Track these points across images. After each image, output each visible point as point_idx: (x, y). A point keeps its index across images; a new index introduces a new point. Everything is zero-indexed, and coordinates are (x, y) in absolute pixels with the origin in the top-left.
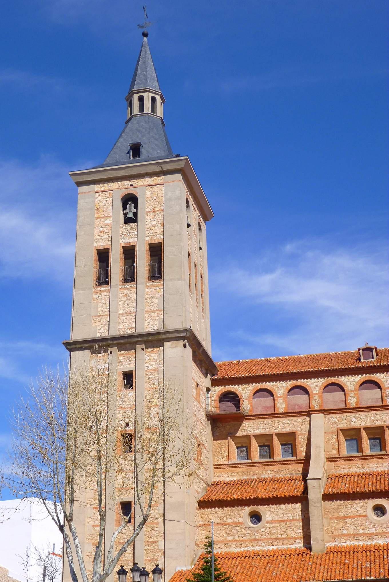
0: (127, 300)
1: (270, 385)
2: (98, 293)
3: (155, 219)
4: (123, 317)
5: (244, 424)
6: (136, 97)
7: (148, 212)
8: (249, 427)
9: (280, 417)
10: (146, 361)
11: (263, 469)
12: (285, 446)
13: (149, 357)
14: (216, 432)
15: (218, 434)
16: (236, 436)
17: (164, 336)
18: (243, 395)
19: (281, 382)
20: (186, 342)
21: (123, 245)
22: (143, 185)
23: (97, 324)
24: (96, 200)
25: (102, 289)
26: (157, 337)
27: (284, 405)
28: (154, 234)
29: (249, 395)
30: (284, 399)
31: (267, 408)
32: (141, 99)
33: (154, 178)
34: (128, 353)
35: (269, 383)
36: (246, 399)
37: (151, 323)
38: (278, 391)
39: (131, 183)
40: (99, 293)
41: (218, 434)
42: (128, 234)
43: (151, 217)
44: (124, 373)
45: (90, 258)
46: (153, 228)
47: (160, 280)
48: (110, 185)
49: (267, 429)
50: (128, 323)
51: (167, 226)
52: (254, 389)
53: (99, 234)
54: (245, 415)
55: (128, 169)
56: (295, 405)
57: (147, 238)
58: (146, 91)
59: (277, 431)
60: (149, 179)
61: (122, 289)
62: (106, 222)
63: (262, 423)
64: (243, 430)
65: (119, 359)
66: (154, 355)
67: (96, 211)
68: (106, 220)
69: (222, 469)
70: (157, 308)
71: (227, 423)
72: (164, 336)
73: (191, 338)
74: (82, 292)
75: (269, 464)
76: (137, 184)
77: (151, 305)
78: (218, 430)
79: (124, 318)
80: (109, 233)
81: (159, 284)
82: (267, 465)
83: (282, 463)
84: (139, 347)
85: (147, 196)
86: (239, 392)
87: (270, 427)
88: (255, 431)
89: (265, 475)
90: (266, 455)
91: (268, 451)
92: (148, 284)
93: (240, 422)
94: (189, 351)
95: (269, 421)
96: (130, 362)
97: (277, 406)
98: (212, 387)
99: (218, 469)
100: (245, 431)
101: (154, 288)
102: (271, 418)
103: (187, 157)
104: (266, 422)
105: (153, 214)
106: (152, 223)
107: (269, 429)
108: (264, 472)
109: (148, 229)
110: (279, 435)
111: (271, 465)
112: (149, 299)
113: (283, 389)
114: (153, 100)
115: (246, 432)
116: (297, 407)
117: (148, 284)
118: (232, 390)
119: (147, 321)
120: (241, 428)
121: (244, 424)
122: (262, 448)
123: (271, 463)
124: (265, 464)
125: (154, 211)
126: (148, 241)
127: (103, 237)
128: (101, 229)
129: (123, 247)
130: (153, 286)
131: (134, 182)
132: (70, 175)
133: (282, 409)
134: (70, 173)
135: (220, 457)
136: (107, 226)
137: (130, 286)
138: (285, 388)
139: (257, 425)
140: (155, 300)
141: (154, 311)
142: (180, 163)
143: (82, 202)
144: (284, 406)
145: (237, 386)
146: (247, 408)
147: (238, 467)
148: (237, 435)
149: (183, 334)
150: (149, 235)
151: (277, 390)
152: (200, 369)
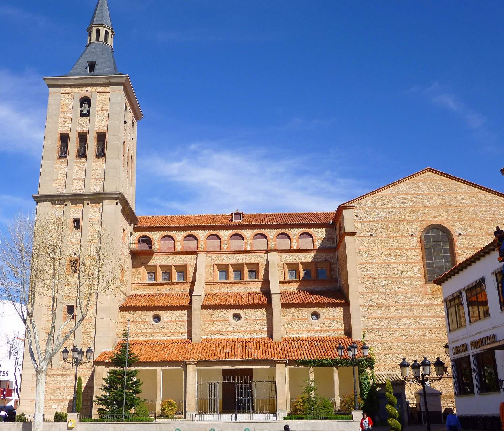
1: (172, 233)
15: (136, 263)
17: (103, 196)
18: (154, 239)
21: (79, 132)
23: (57, 185)
25: (62, 161)
26: (98, 197)
30: (181, 243)
31: (169, 248)
38: (178, 238)
41: (136, 263)
42: (83, 125)
46: (101, 122)
48: (72, 89)
55: (86, 79)
56: (188, 247)
60: (100, 88)
62: (68, 115)
78: (136, 260)
79: (77, 182)
82: (166, 285)
84: (86, 202)
91: (168, 276)
94: (120, 207)
95: (170, 256)
97: (176, 247)
105: (101, 112)
106: (100, 118)
108: (165, 289)
114: (106, 33)
115: (155, 263)
125: (102, 110)
128: (64, 120)
134: (44, 78)
137: (82, 160)
140: (99, 171)
141: (98, 179)
144: (181, 247)
149: (117, 196)
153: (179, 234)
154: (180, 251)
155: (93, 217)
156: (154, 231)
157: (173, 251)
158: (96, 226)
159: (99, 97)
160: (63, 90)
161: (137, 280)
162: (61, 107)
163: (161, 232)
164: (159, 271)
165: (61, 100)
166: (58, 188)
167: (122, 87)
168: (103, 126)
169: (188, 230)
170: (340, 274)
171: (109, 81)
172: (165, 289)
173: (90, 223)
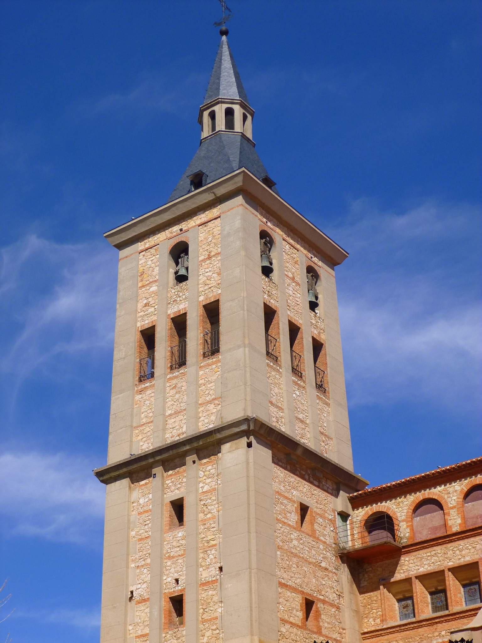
0: (176, 393)
1: (436, 492)
2: (140, 392)
3: (210, 269)
4: (171, 420)
5: (402, 561)
6: (206, 114)
7: (202, 260)
8: (411, 565)
9: (454, 541)
10: (201, 479)
11: (434, 630)
12: (468, 588)
13: (204, 472)
14: (363, 579)
15: (366, 583)
16: (391, 581)
17: (219, 436)
18: (399, 514)
19: (453, 484)
20: (252, 438)
21: (172, 316)
22: (195, 226)
23: (140, 437)
24: (140, 263)
25: (146, 385)
26: (210, 439)
27: (459, 519)
28: (209, 290)
29: (408, 512)
30: (458, 511)
31: (435, 529)
32: (213, 116)
33: (208, 212)
34: (178, 472)
35: (435, 488)
36: (403, 521)
37: (206, 421)
38: (449, 499)
39: (180, 227)
40: (142, 392)
41: (366, 583)
42: (178, 299)
43: (206, 266)
44: (173, 503)
45: (131, 344)
46: (208, 282)
47: (217, 354)
48: (156, 238)
49: (437, 564)
50: (177, 427)
51: (225, 274)
52: (413, 502)
53: (144, 309)
54: (401, 546)
55: (174, 209)
56: (477, 518)
57: (201, 298)
58: (218, 103)
59: (452, 563)
60: (203, 216)
61: (170, 379)
62: (152, 289)
63: (429, 554)
64: (402, 571)
65: (166, 484)
66: (210, 467)
67: (139, 279)
68: (151, 287)
69: (374, 639)
70: (213, 397)
71: (378, 564)
72: (219, 436)
73: (262, 432)
74: (120, 396)
75: (442, 619)
76: (188, 226)
77: (206, 393)
78: (366, 576)
79: (173, 420)
80: (154, 305)
81: (215, 361)
82: (439, 622)
83: (461, 615)
84: (189, 459)
85: (200, 239)
86: (392, 512)
87: (441, 559)
88: (419, 569)
89: (437, 639)
90: (441, 607)
91: (443, 599)
92: (202, 364)
93: (396, 559)
94: (265, 454)
95: (438, 549)
96: (179, 486)
97: (450, 523)
98: (353, 511)
99: (368, 640)
100: (404, 572)
101: (210, 367)
102: (441, 545)
103: (243, 169)
104: (434, 552)
105: (208, 262)
106: (207, 274)
107: (439, 563)
108: (437, 634)
109: (202, 286)
110: (454, 570)
111: (446, 621)
112: (204, 385)
113: (456, 495)
114: (229, 113)
115: (406, 574)
116: (479, 519)
117: (202, 364)
118: (382, 509)
119: (201, 419)
120: (398, 568)
121: (402, 561)
122: (435, 596)
123: (446, 618)
124: (437, 621)
125: (209, 258)
126: (202, 302)
127: (149, 311)
128: (145, 302)
129: (172, 319)
130: (209, 365)
131: (184, 225)
132: (105, 237)
133: (456, 526)
134: (105, 235)
135: (371, 620)
136: (153, 295)
137: (180, 372)
138: (459, 492)
139: (422, 558)
140: (211, 385)
141: (210, 402)
142: (236, 179)
143: (123, 270)
144: (459, 521)
145: (388, 502)
146: (404, 535)
147: (398, 631)
148: (392, 580)
149: (244, 427)
150: (203, 293)
151: (448, 497)
152: (316, 483)
153: (451, 490)
154: (459, 530)
155: (206, 488)
156: (395, 498)
157: (446, 534)
158: (213, 507)
159: (202, 234)
160: (141, 246)
161: (373, 623)
162: (139, 279)
163: (411, 495)
164: (419, 589)
165: (140, 266)
166: (141, 444)
167: (240, 197)
168: (212, 288)
169: (470, 475)
170: (133, 371)
171: (215, 195)
172: (437, 634)
173: (202, 503)
